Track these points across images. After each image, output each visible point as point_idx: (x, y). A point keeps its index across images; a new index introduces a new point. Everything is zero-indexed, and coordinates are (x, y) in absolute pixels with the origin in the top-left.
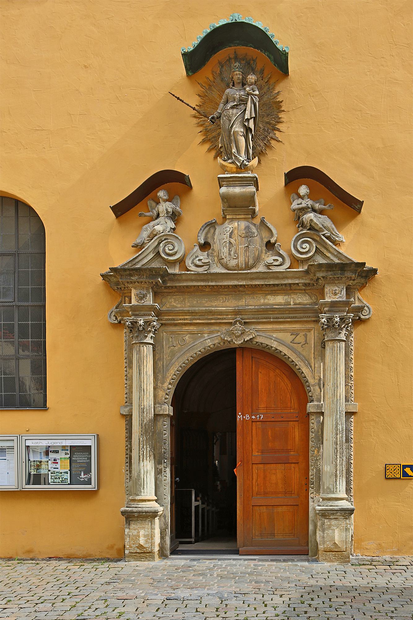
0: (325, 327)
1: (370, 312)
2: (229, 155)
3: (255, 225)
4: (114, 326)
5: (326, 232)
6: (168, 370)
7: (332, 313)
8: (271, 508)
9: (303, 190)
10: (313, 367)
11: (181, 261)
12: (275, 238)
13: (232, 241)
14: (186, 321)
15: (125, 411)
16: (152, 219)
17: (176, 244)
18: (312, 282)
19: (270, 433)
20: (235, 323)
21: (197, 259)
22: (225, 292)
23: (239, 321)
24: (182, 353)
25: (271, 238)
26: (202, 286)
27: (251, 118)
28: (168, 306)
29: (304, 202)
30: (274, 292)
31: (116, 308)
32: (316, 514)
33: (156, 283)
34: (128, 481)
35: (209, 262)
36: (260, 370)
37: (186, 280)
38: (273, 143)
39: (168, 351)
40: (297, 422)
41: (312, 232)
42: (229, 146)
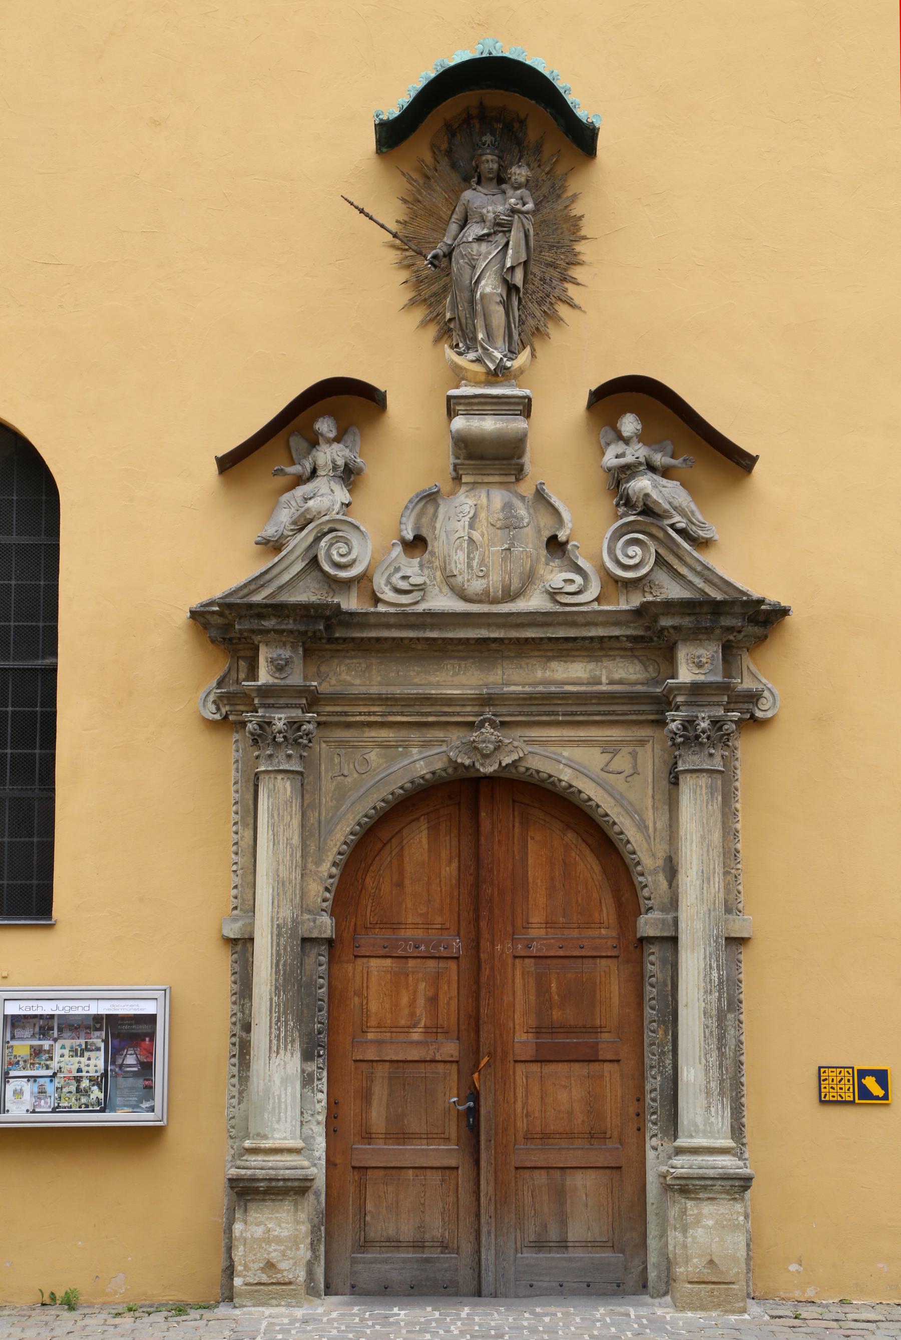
0: (680, 740)
1: (774, 703)
2: (471, 342)
3: (523, 498)
4: (212, 725)
6: (330, 832)
7: (695, 709)
8: (558, 1173)
9: (629, 424)
11: (364, 578)
12: (568, 532)
13: (476, 535)
14: (373, 719)
15: (233, 930)
16: (299, 480)
17: (355, 543)
18: (649, 633)
19: (553, 985)
20: (482, 724)
22: (459, 651)
23: (489, 720)
24: (362, 791)
25: (558, 529)
26: (411, 639)
28: (333, 682)
29: (629, 450)
30: (564, 653)
31: (220, 685)
32: (667, 1188)
33: (314, 633)
34: (234, 1101)
35: (425, 583)
36: (531, 834)
37: (377, 626)
38: (563, 310)
39: (332, 786)
40: (615, 960)
41: (648, 520)
42: (470, 321)
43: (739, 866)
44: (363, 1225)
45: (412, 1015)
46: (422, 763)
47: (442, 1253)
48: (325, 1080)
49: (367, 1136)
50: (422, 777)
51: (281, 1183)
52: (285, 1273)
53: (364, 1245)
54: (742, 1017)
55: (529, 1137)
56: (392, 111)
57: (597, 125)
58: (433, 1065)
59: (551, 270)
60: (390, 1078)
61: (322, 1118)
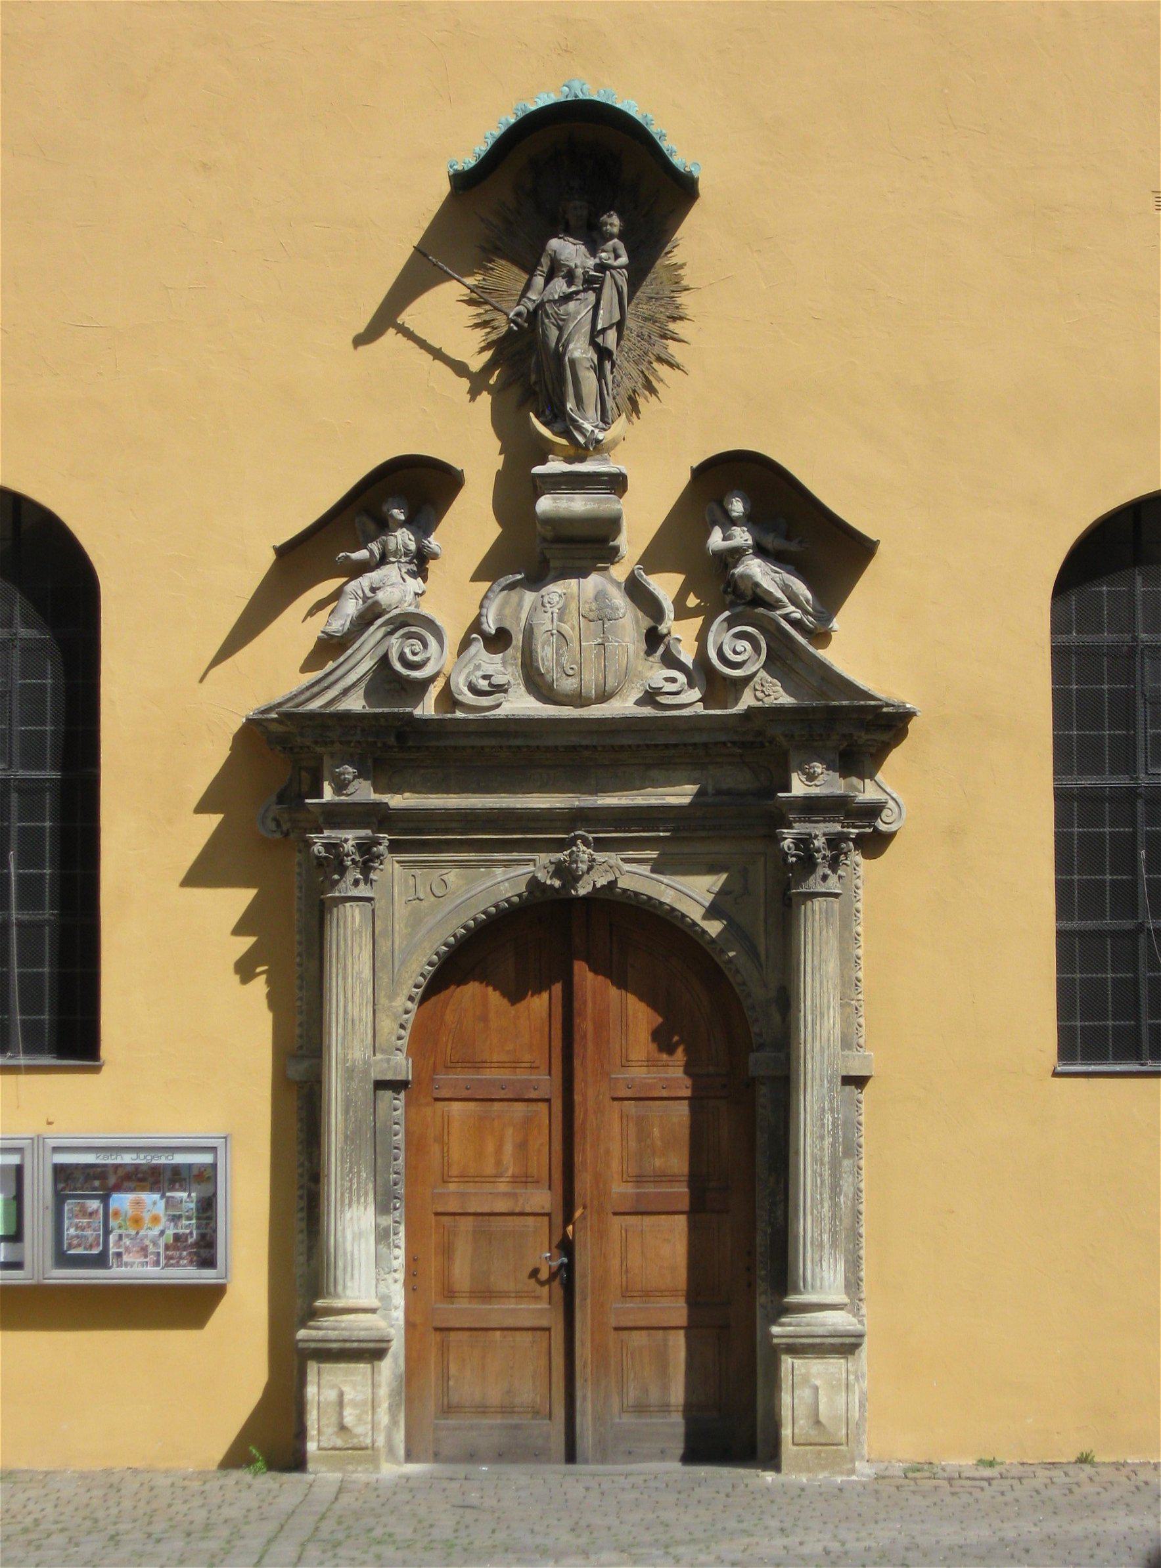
5: (792, 608)
10: (763, 957)
13: (566, 628)
21: (480, 673)
27: (610, 327)
43: (860, 997)
44: (446, 1390)
45: (498, 1163)
46: (506, 884)
47: (534, 1418)
48: (402, 1234)
49: (449, 1294)
50: (507, 900)
51: (355, 1345)
52: (362, 1439)
53: (448, 1409)
54: (862, 1163)
55: (626, 1294)
56: (467, 161)
57: (696, 175)
58: (521, 1218)
59: (649, 324)
60: (474, 1231)
61: (401, 1276)
